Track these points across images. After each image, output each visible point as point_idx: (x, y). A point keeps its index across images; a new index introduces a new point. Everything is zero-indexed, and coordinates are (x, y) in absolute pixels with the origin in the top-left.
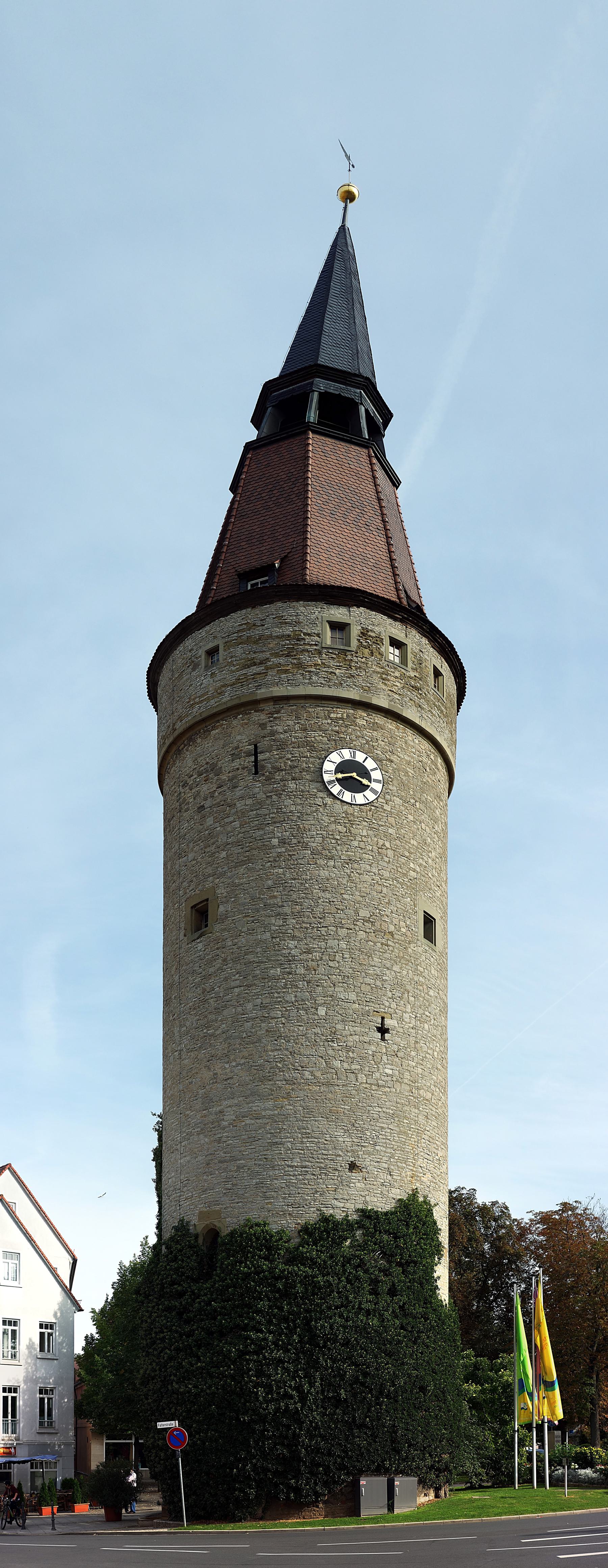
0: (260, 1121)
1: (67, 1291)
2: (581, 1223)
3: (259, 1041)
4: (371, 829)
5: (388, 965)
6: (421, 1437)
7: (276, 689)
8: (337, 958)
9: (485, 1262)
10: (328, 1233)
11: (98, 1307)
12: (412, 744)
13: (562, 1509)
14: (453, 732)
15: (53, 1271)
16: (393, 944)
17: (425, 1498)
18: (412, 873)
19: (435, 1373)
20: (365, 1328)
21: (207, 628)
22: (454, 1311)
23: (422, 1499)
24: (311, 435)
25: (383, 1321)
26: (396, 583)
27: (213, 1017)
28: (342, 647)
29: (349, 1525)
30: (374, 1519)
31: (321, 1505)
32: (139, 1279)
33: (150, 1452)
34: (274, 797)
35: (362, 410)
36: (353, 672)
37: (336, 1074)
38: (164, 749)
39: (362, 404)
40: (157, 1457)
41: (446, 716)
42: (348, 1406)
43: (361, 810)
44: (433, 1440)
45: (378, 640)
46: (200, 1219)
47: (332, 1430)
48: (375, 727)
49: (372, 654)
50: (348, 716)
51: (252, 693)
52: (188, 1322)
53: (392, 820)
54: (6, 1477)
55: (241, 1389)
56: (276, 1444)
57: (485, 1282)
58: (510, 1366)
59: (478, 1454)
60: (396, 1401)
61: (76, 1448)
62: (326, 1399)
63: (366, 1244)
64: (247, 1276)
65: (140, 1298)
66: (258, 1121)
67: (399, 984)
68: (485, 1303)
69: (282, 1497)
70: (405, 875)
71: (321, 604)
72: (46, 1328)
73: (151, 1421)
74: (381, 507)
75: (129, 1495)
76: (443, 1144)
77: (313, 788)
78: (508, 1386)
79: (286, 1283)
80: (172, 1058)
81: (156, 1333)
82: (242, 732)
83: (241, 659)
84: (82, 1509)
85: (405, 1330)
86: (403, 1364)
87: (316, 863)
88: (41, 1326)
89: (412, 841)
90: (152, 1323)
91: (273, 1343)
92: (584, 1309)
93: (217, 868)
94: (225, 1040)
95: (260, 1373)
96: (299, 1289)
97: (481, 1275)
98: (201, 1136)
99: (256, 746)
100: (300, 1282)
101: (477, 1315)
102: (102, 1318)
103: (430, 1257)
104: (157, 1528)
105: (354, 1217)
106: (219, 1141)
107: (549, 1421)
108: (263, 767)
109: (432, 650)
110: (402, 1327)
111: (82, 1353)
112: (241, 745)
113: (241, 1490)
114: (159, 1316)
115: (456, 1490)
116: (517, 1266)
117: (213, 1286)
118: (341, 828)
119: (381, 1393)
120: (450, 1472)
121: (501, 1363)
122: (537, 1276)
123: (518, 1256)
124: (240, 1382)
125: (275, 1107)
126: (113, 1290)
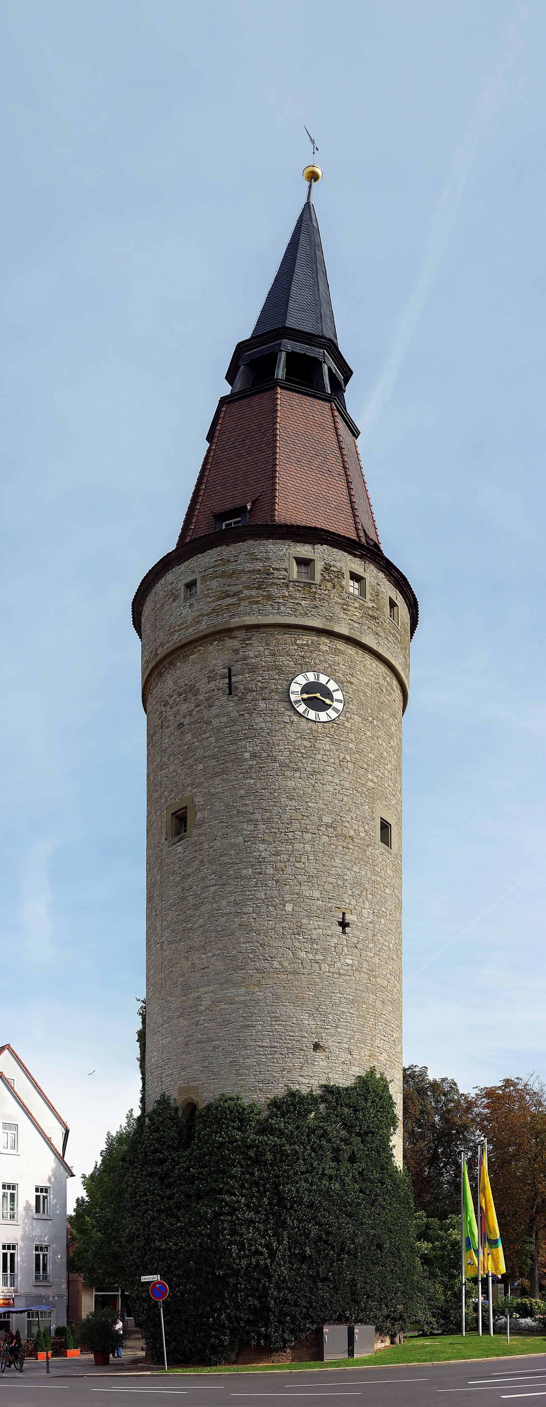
0: (234, 1006)
1: (61, 1158)
2: (522, 1098)
3: (233, 934)
4: (334, 744)
5: (349, 866)
6: (378, 1289)
7: (248, 618)
8: (303, 860)
9: (436, 1133)
10: (295, 1106)
11: (88, 1172)
12: (370, 667)
13: (505, 1354)
14: (407, 656)
15: (48, 1141)
16: (353, 847)
17: (382, 1344)
18: (370, 784)
19: (391, 1232)
20: (328, 1192)
21: (186, 563)
22: (407, 1176)
23: (379, 1345)
24: (279, 390)
25: (344, 1185)
26: (356, 523)
27: (190, 912)
28: (307, 581)
29: (313, 1368)
30: (335, 1363)
31: (288, 1351)
32: (125, 1148)
33: (134, 1303)
34: (246, 715)
35: (325, 368)
36: (317, 603)
37: (302, 964)
38: (147, 672)
39: (325, 362)
40: (141, 1309)
41: (400, 643)
42: (312, 1262)
43: (324, 727)
44: (388, 1292)
45: (340, 574)
46: (179, 1094)
47: (298, 1283)
48: (337, 652)
49: (334, 587)
50: (312, 642)
51: (226, 622)
52: (169, 1186)
53: (352, 736)
54: (5, 1326)
55: (217, 1246)
56: (247, 1296)
57: (436, 1150)
58: (458, 1226)
59: (429, 1305)
60: (356, 1257)
61: (68, 1300)
62: (293, 1255)
63: (329, 1116)
64: (222, 1145)
65: (126, 1165)
66: (231, 1006)
67: (358, 883)
68: (436, 1169)
69: (253, 1343)
70: (364, 785)
71: (288, 542)
72: (42, 1191)
73: (136, 1275)
74: (342, 455)
75: (115, 1342)
76: (398, 1026)
77: (281, 707)
78: (456, 1244)
79: (257, 1151)
80: (154, 949)
81: (140, 1196)
82: (217, 656)
83: (216, 592)
84: (74, 1354)
85: (364, 1194)
86: (362, 1224)
87: (284, 775)
88: (37, 1190)
89: (370, 755)
90: (136, 1187)
91: (246, 1205)
92: (524, 1175)
93: (195, 779)
94: (202, 933)
95: (233, 1232)
96: (269, 1156)
97: (432, 1145)
98: (181, 1019)
99: (230, 670)
100: (269, 1151)
101: (428, 1180)
102: (92, 1183)
103: (386, 1128)
104: (141, 1371)
105: (318, 1092)
106: (197, 1024)
107: (493, 1275)
108: (237, 688)
109: (388, 583)
110: (361, 1191)
111: (74, 1214)
112: (216, 669)
113: (217, 1337)
114: (143, 1181)
115: (410, 1337)
116: (464, 1136)
117: (191, 1154)
118: (306, 743)
119: (342, 1250)
120: (404, 1321)
121: (450, 1223)
122: (482, 1145)
123: (465, 1127)
124: (216, 1240)
125: (247, 993)
126: (101, 1158)
